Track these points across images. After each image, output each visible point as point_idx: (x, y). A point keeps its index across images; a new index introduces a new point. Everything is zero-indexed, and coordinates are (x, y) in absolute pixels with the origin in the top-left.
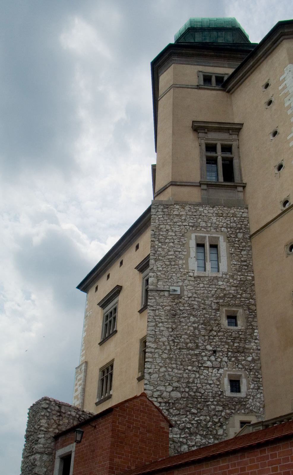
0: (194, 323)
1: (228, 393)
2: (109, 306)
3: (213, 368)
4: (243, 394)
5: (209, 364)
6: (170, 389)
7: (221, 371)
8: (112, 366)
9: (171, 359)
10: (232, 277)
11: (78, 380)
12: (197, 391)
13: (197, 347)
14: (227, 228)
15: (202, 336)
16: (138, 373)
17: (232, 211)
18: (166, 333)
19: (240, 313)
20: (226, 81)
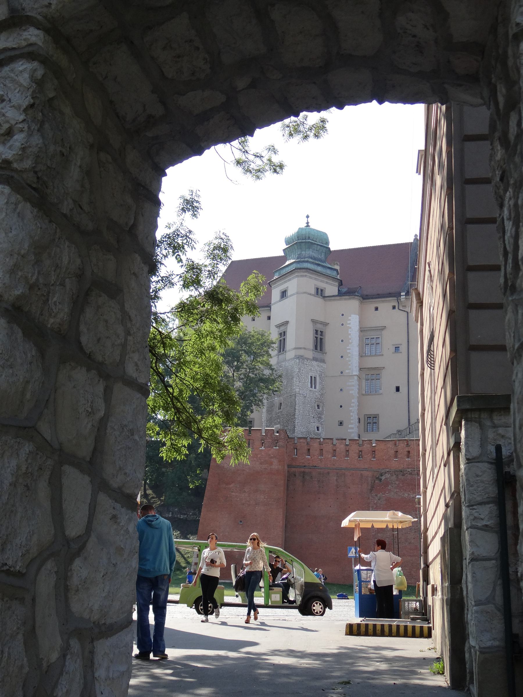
0: (309, 407)
1: (316, 431)
2: (453, 518)
3: (313, 422)
4: (320, 432)
5: (312, 421)
6: (302, 428)
7: (315, 424)
8: (286, 291)
9: (303, 418)
10: (319, 391)
11: (147, 671)
12: (309, 429)
13: (309, 415)
14: (319, 371)
15: (401, 476)
16: (348, 599)
17: (321, 365)
18: (302, 409)
19: (321, 405)
20: (172, 670)
